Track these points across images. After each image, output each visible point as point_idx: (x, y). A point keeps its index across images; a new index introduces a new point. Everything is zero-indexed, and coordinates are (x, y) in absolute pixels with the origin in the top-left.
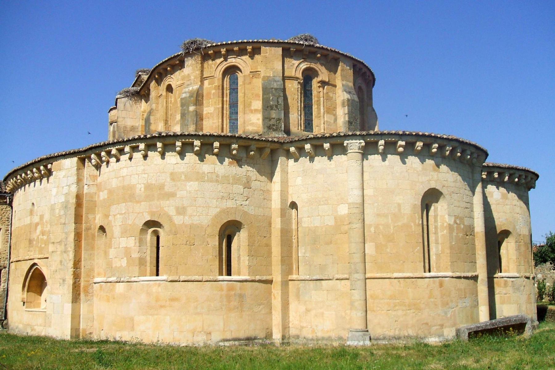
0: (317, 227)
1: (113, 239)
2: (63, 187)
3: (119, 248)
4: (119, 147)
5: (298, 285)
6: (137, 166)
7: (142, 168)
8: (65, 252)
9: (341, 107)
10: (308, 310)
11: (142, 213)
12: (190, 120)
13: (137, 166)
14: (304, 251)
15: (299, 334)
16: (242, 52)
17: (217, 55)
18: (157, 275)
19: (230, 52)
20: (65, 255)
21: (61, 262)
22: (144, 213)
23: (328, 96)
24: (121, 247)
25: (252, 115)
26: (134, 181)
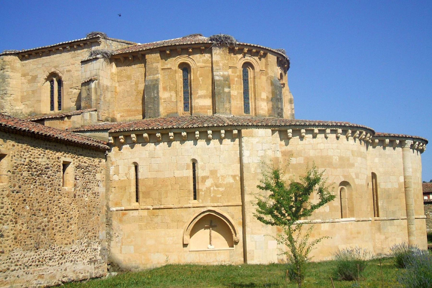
0: (389, 189)
2: (257, 151)
4: (321, 128)
5: (379, 223)
6: (332, 143)
7: (336, 145)
9: (288, 103)
10: (386, 238)
11: (339, 175)
12: (225, 98)
13: (332, 143)
14: (382, 202)
15: (381, 252)
16: (257, 54)
17: (241, 51)
18: (342, 218)
19: (250, 52)
25: (262, 102)
26: (330, 153)
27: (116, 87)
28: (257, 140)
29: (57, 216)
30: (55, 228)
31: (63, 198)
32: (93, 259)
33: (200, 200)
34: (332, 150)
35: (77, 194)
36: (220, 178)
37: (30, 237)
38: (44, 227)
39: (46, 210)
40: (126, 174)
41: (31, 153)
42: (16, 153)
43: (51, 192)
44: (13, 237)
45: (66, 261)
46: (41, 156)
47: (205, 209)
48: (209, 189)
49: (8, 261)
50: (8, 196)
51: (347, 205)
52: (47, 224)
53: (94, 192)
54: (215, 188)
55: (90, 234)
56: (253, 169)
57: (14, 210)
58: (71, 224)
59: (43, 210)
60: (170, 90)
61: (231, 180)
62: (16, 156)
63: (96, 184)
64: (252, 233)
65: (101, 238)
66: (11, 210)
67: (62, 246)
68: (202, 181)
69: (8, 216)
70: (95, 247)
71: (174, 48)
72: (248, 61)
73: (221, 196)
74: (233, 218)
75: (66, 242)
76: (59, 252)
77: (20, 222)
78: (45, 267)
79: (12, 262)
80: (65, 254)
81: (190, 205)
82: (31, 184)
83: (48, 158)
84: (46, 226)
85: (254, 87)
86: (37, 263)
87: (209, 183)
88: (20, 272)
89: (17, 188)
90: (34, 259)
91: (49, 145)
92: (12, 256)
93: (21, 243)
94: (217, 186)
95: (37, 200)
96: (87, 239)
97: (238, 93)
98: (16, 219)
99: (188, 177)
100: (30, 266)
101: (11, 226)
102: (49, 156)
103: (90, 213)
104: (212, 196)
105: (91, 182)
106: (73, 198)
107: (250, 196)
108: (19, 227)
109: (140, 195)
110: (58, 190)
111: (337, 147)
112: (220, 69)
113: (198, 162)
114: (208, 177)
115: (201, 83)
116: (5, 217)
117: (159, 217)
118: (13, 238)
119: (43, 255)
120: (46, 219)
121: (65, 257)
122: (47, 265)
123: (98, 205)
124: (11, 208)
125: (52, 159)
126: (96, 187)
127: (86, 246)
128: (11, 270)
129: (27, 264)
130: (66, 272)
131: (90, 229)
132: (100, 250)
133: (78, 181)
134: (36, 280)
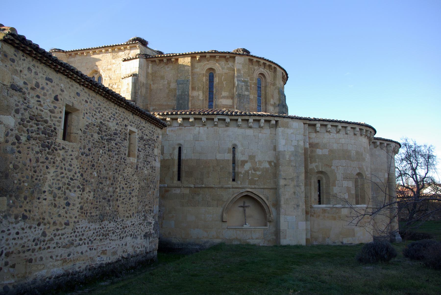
3: (342, 187)
21: (294, 193)
26: (350, 148)
27: (150, 85)
28: (292, 131)
29: (121, 187)
30: (119, 199)
31: (127, 168)
33: (239, 182)
34: (351, 145)
35: (139, 166)
36: (258, 163)
37: (97, 208)
38: (109, 198)
39: (112, 179)
40: (171, 154)
41: (102, 114)
42: (89, 111)
43: (117, 160)
44: (79, 206)
45: (127, 235)
46: (111, 120)
47: (244, 190)
48: (247, 172)
49: (73, 234)
50: (77, 158)
52: (112, 194)
53: (152, 165)
54: (253, 172)
56: (287, 157)
57: (82, 175)
58: (133, 197)
59: (110, 179)
60: (198, 90)
61: (267, 166)
62: (88, 114)
64: (285, 214)
66: (79, 175)
67: (124, 218)
68: (241, 165)
69: (75, 181)
70: (150, 221)
71: (203, 55)
74: (267, 200)
75: (128, 215)
76: (121, 226)
77: (87, 189)
78: (108, 241)
79: (76, 236)
80: (126, 227)
81: (230, 186)
82: (101, 148)
83: (117, 124)
84: (111, 196)
85: (266, 94)
86: (101, 237)
87: (247, 166)
88: (84, 248)
89: (86, 151)
90: (98, 233)
91: (119, 110)
92: (77, 228)
93: (87, 213)
94: (255, 170)
95: (105, 167)
97: (254, 97)
98: (84, 185)
99: (228, 160)
100: (95, 240)
101: (79, 193)
102: (118, 122)
105: (151, 155)
106: (136, 170)
107: (284, 180)
108: (86, 195)
109: (183, 174)
110: (124, 159)
111: (355, 143)
113: (239, 147)
114: (246, 162)
115: (225, 86)
116: (72, 182)
117: (201, 195)
118: (79, 207)
119: (106, 228)
120: (111, 189)
121: (126, 231)
122: (110, 240)
124: (79, 172)
125: (121, 125)
126: (154, 162)
128: (75, 245)
129: (91, 238)
130: (127, 247)
133: (141, 153)
134: (99, 256)
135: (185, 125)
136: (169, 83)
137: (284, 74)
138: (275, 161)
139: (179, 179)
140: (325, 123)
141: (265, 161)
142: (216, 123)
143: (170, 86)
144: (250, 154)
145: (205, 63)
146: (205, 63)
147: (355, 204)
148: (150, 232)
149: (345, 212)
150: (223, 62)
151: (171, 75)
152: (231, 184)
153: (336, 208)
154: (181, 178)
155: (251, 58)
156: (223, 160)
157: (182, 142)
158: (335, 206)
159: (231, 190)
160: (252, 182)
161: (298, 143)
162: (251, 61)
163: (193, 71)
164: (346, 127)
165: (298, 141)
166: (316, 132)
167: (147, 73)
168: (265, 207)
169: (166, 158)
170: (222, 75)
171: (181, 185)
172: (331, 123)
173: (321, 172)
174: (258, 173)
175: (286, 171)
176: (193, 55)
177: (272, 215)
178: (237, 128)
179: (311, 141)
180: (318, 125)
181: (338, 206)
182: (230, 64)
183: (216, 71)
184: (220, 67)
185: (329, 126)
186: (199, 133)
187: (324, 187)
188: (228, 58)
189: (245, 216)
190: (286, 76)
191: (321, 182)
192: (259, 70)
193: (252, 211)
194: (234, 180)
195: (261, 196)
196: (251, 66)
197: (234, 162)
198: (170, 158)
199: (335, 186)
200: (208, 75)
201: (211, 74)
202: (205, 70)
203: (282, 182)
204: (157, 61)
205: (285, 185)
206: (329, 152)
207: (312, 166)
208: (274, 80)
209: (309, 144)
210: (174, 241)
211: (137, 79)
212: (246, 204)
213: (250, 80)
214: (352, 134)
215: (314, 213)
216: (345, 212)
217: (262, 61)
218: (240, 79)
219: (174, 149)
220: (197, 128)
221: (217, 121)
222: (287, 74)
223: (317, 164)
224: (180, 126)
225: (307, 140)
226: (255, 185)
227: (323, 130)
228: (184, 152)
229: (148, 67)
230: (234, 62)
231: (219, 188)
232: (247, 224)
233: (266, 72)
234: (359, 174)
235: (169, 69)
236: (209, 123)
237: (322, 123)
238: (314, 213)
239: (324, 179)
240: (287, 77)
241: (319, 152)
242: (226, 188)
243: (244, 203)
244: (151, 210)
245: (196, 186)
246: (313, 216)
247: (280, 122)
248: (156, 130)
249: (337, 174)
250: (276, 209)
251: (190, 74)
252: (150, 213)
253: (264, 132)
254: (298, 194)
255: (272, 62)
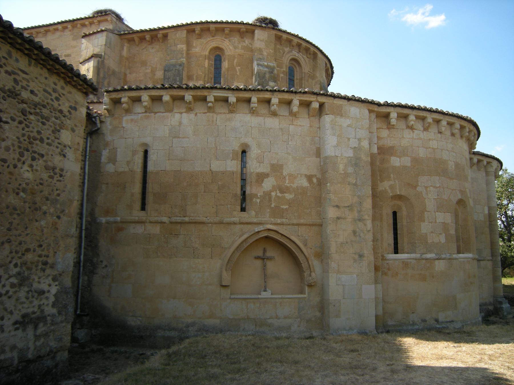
1: (426, 213)
2: (349, 139)
3: (436, 222)
8: (360, 220)
11: (455, 190)
13: (447, 142)
20: (360, 224)
21: (354, 232)
22: (38, 334)
23: (234, 380)
24: (437, 221)
26: (445, 156)
27: (125, 75)
28: (348, 122)
32: (33, 316)
36: (287, 178)
40: (128, 163)
47: (261, 228)
48: (268, 194)
51: (460, 234)
54: (279, 194)
55: (29, 256)
56: (341, 167)
61: (305, 183)
63: (59, 150)
65: (60, 267)
71: (206, 26)
72: (296, 57)
73: (287, 207)
74: (306, 245)
81: (236, 219)
87: (268, 184)
94: (282, 192)
96: (18, 269)
103: (36, 209)
104: (273, 206)
107: (336, 209)
109: (150, 198)
112: (264, 59)
113: (252, 149)
114: (267, 175)
115: (238, 73)
123: (58, 195)
127: (13, 285)
131: (31, 247)
132: (55, 295)
135: (156, 111)
136: (153, 72)
137: (328, 65)
138: (319, 176)
139: (143, 208)
140: (406, 111)
141: (301, 175)
142: (210, 104)
143: (155, 75)
144: (273, 162)
145: (209, 39)
146: (209, 39)
147: (456, 252)
148: (42, 311)
149: (440, 266)
150: (236, 39)
151: (156, 59)
152: (238, 216)
153: (426, 259)
154: (146, 207)
155: (280, 34)
156: (223, 173)
157: (148, 140)
158: (424, 256)
159: (238, 227)
160: (277, 212)
161: (359, 144)
162: (279, 38)
163: (190, 52)
164: (438, 122)
165: (359, 140)
166: (390, 127)
167: (121, 57)
168: (301, 258)
169: (121, 170)
170: (234, 57)
171: (144, 218)
172: (415, 112)
173: (400, 197)
174: (289, 196)
175: (340, 193)
176: (189, 27)
177: (313, 274)
178: (250, 115)
179: (381, 143)
180: (394, 115)
181: (429, 256)
182: (246, 42)
183: (226, 51)
184: (231, 47)
185: (412, 118)
186: (180, 123)
187: (405, 223)
188: (243, 32)
189: (265, 275)
190: (330, 70)
191: (398, 215)
192: (291, 54)
193: (279, 266)
194: (243, 209)
195: (293, 238)
196: (278, 46)
197: (243, 180)
198: (127, 169)
199: (424, 221)
200: (213, 58)
201: (217, 57)
202: (208, 50)
203: (331, 213)
204: (136, 39)
205: (338, 218)
206: (411, 162)
207: (385, 185)
208: (314, 71)
209: (378, 149)
210: (132, 322)
211: (103, 62)
212: (269, 254)
213: (278, 67)
214: (448, 133)
215: (389, 269)
216: (440, 266)
217: (296, 40)
218: (261, 63)
219: (134, 153)
220: (177, 116)
221: (213, 100)
222: (332, 68)
223: (391, 183)
224: (146, 112)
225: (375, 140)
226: (282, 217)
227: (402, 124)
228: (152, 157)
229: (123, 49)
230: (253, 38)
231: (215, 223)
232: (267, 289)
233: (301, 57)
234: (461, 202)
235: (153, 51)
236: (200, 108)
237: (400, 110)
238: (389, 269)
239: (404, 209)
240: (333, 73)
241: (395, 161)
242: (229, 224)
243: (265, 251)
244: (45, 263)
245: (174, 219)
246: (386, 274)
247: (326, 105)
248: (70, 93)
249: (426, 200)
250: (322, 261)
251: (185, 55)
252: (44, 270)
253: (299, 123)
254: (362, 235)
255: (311, 44)
